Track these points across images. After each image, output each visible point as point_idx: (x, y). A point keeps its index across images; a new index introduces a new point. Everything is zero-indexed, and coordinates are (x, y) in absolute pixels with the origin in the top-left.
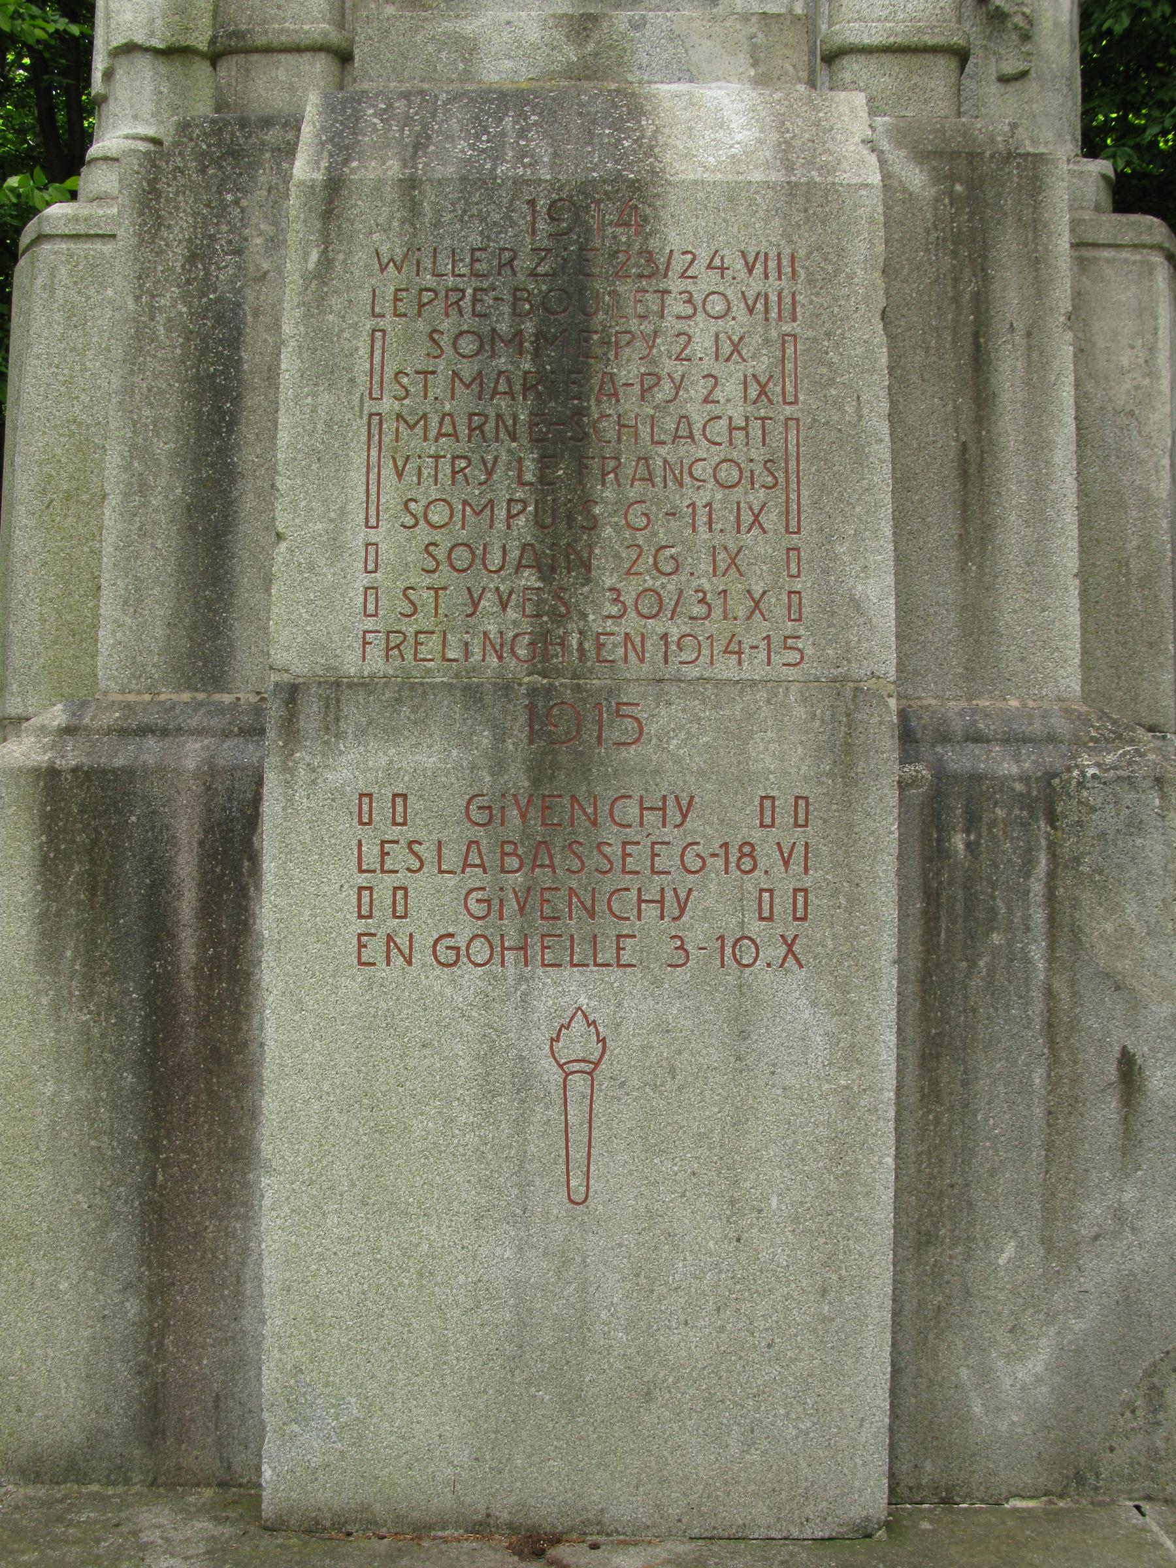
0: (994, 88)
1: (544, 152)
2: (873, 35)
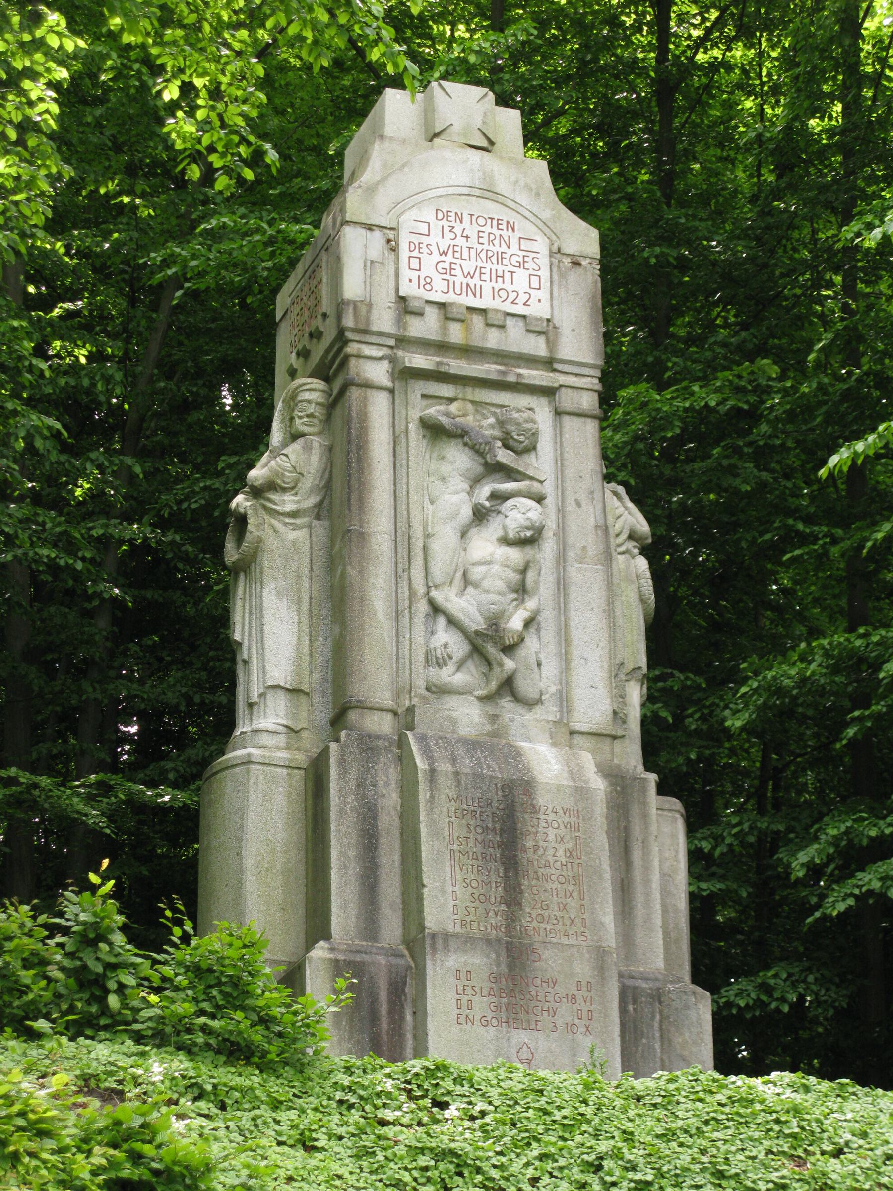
2: (585, 728)
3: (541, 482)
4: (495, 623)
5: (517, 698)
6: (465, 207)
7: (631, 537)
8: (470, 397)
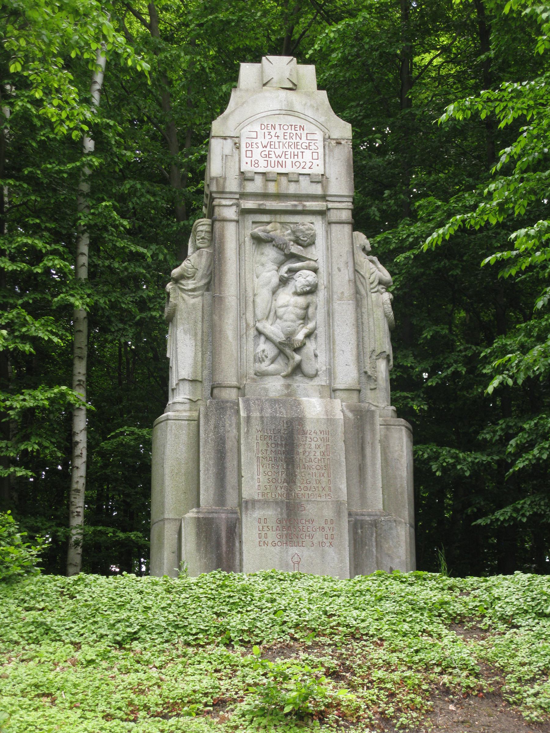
0: (369, 391)
1: (284, 412)
3: (316, 261)
4: (290, 336)
5: (305, 375)
6: (276, 121)
7: (380, 283)
8: (278, 220)
